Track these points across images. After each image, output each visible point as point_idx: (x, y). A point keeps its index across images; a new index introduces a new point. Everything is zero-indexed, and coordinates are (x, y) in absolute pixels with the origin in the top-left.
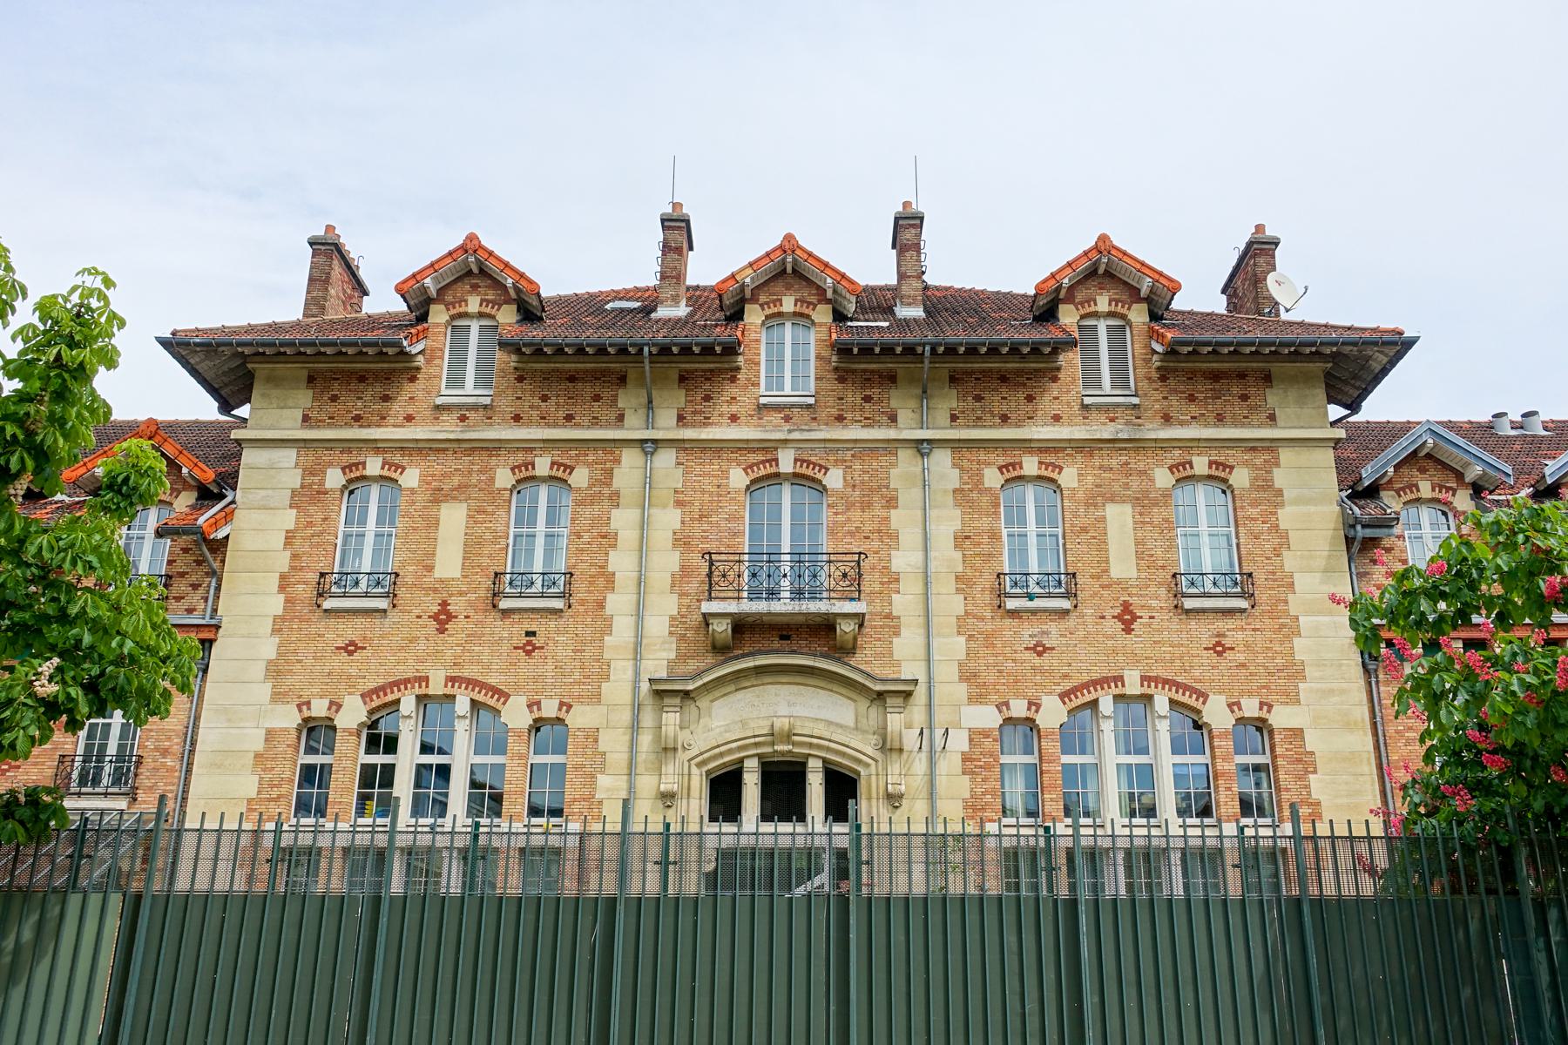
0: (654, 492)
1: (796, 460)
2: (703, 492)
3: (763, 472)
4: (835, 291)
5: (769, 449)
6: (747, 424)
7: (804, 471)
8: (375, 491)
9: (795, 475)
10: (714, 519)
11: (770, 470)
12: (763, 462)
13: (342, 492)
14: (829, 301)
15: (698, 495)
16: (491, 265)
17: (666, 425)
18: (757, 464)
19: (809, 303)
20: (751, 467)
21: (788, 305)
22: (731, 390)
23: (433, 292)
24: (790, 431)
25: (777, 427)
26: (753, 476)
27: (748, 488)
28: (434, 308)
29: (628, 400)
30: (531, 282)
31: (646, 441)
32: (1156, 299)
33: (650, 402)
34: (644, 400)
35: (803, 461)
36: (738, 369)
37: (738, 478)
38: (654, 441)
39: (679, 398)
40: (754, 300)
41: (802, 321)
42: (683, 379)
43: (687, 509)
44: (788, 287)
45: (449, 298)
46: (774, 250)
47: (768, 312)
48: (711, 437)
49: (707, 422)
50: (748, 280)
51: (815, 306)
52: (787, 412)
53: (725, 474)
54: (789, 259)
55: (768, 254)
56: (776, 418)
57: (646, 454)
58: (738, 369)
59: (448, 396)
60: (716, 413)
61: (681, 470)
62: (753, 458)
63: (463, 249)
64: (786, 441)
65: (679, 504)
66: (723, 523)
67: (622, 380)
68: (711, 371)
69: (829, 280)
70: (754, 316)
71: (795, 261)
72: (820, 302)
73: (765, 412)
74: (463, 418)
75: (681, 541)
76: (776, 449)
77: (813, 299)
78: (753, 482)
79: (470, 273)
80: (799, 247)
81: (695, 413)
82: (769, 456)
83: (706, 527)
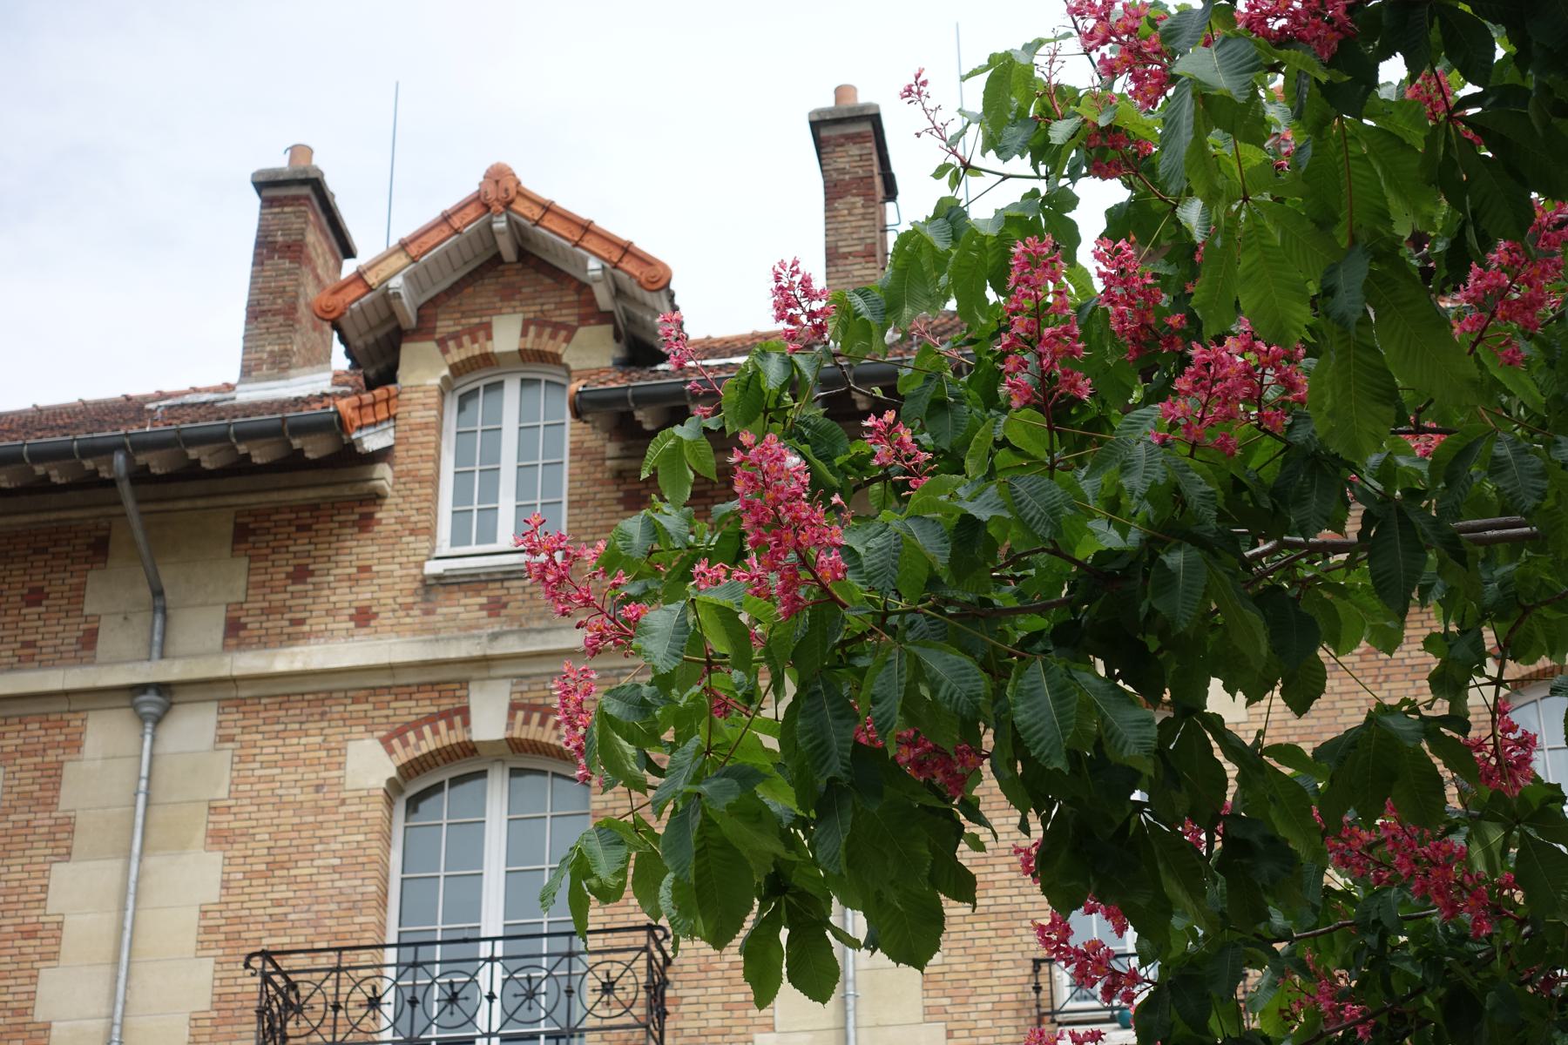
0: (158, 814)
1: (514, 708)
2: (280, 805)
3: (429, 744)
4: (619, 292)
5: (444, 684)
6: (397, 629)
7: (533, 732)
8: (496, 796)
9: (516, 746)
10: (303, 871)
11: (448, 737)
12: (431, 719)
13: (390, 803)
14: (606, 317)
15: (269, 813)
16: (551, 234)
17: (200, 650)
18: (416, 726)
19: (557, 327)
20: (400, 733)
21: (506, 336)
22: (361, 549)
23: (408, 308)
24: (494, 637)
25: (468, 629)
26: (403, 756)
27: (394, 788)
28: (408, 351)
29: (109, 596)
30: (645, 261)
31: (142, 688)
32: (625, 301)
33: (158, 593)
34: (145, 593)
35: (532, 708)
36: (377, 497)
37: (370, 764)
38: (163, 688)
39: (229, 580)
40: (423, 330)
41: (543, 373)
42: (242, 534)
43: (237, 850)
44: (509, 294)
45: (445, 326)
46: (461, 208)
47: (456, 355)
48: (298, 666)
49: (295, 632)
50: (396, 283)
51: (571, 331)
52: (496, 590)
53: (336, 756)
54: (500, 224)
55: (446, 218)
56: (468, 607)
57: (142, 719)
58: (377, 497)
59: (446, 553)
60: (319, 610)
61: (227, 752)
62: (407, 710)
63: (480, 202)
64: (485, 661)
65: (218, 838)
66: (324, 880)
67: (98, 549)
68: (314, 507)
69: (594, 264)
70: (423, 372)
71: (516, 228)
72: (584, 320)
73: (439, 595)
74: (495, 608)
75: (216, 930)
76: (464, 683)
77: (568, 316)
78: (410, 770)
79: (495, 261)
80: (522, 194)
81: (267, 612)
82: (446, 704)
83: (282, 892)
